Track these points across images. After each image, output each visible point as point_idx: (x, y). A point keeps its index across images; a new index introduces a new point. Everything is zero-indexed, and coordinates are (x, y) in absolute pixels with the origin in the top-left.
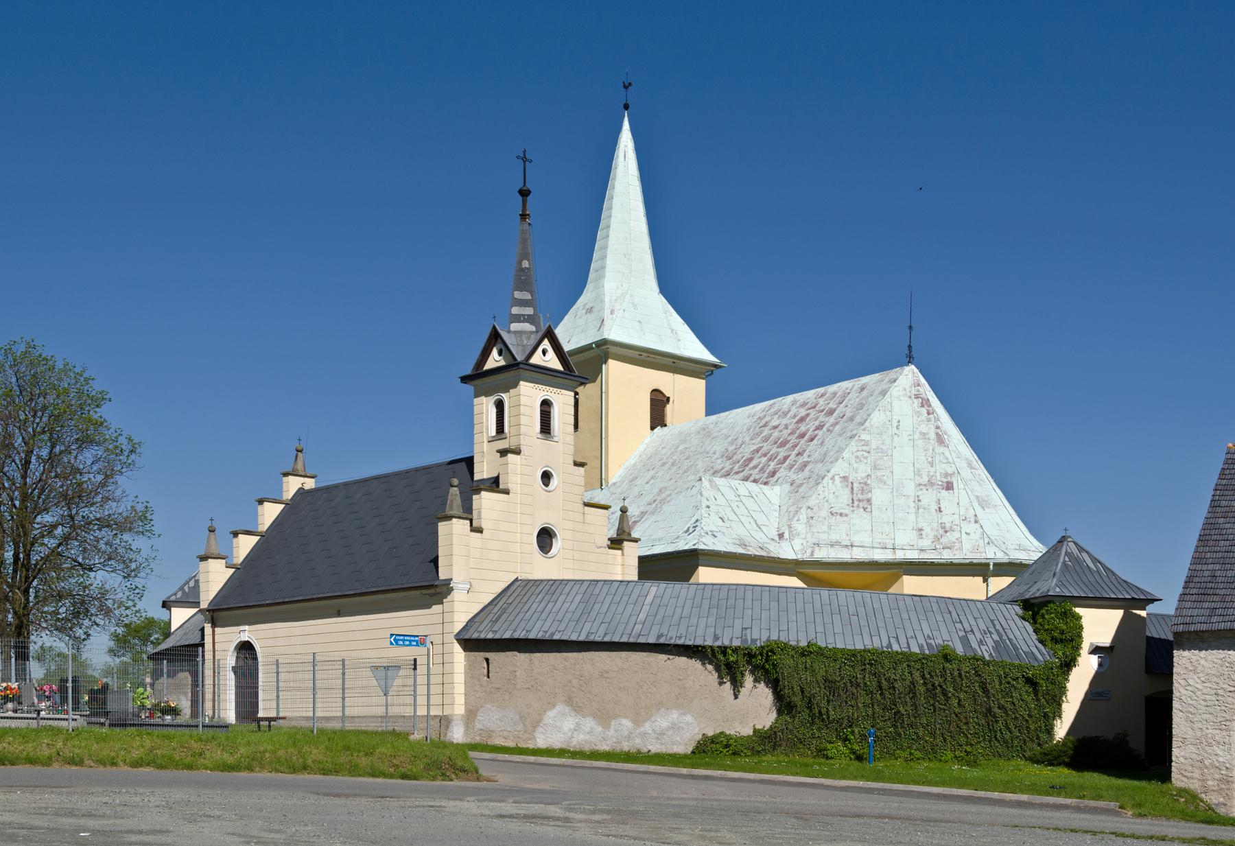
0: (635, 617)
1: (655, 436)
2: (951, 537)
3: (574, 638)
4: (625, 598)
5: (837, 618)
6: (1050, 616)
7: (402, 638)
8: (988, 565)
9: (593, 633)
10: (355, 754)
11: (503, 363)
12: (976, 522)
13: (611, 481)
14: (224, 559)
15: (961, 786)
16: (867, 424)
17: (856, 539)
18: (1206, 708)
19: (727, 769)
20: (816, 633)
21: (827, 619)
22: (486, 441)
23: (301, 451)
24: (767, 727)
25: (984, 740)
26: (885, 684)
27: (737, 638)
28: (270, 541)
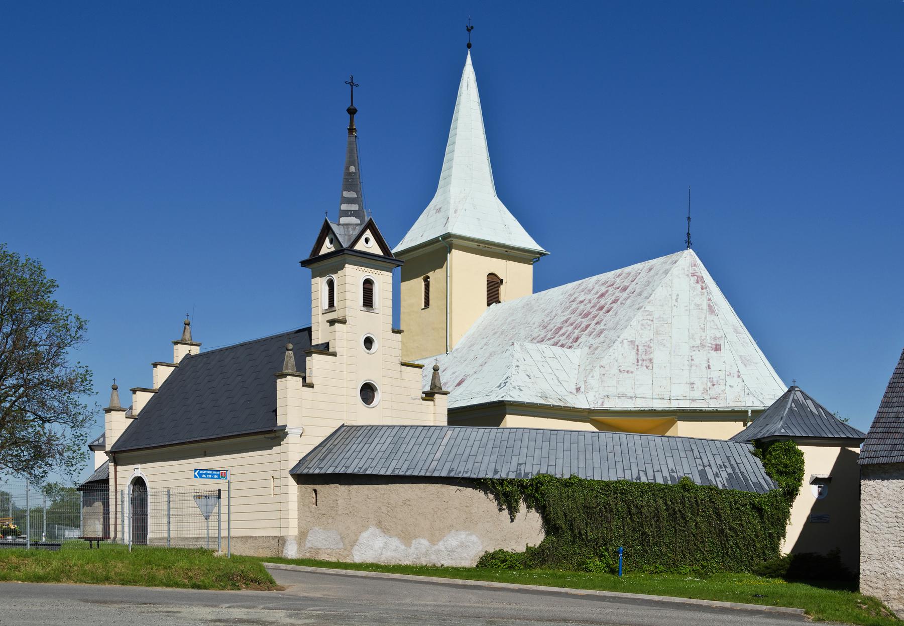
0: (433, 456)
1: (491, 311)
2: (717, 389)
3: (382, 472)
4: (426, 440)
5: (596, 456)
6: (776, 451)
7: (205, 472)
8: (747, 412)
9: (398, 469)
10: (155, 568)
11: (333, 249)
12: (739, 377)
13: (454, 348)
14: (125, 411)
15: (678, 595)
16: (651, 298)
17: (639, 392)
18: (888, 529)
19: (494, 580)
20: (578, 467)
21: (589, 456)
22: (320, 313)
23: (188, 324)
24: (537, 545)
25: (718, 556)
26: (633, 509)
27: (513, 472)
28: (161, 397)
